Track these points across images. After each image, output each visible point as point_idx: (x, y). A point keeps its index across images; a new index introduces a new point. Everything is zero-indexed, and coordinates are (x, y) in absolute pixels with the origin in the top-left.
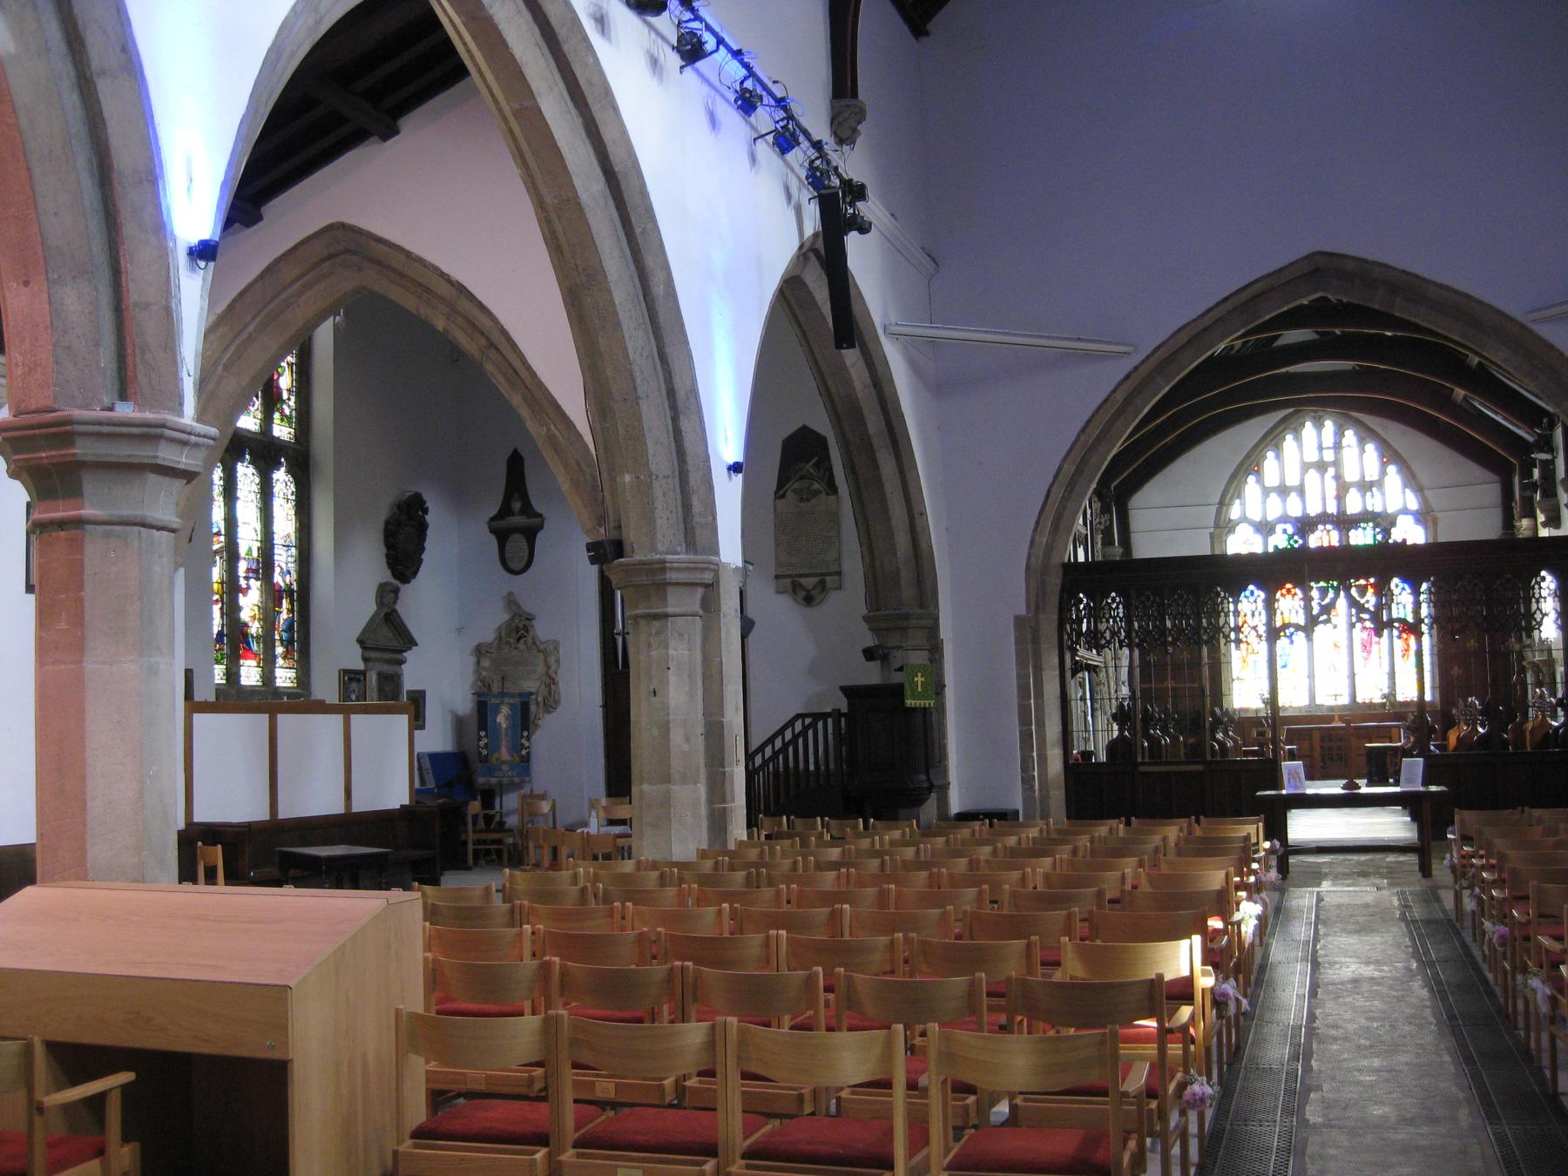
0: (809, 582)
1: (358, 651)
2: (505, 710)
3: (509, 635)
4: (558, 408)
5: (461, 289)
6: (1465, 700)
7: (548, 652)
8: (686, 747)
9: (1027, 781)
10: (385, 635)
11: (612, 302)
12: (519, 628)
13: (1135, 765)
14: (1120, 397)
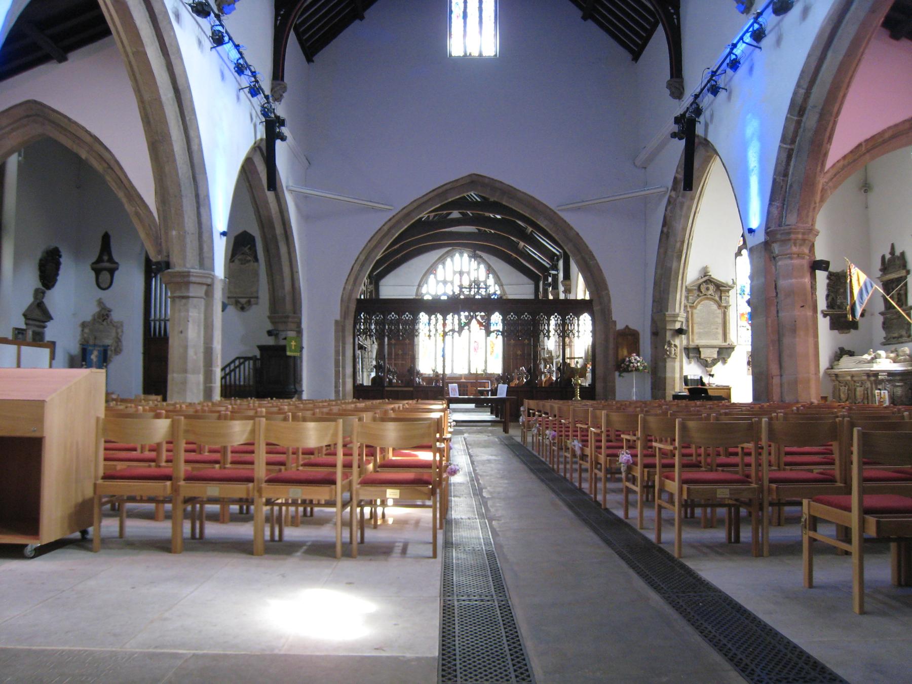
0: (243, 301)
1: (23, 319)
2: (95, 353)
3: (99, 318)
4: (141, 199)
5: (96, 139)
6: (518, 369)
7: (118, 326)
8: (195, 357)
9: (337, 392)
10: (37, 314)
11: (173, 150)
12: (104, 315)
13: (384, 387)
14: (386, 228)
